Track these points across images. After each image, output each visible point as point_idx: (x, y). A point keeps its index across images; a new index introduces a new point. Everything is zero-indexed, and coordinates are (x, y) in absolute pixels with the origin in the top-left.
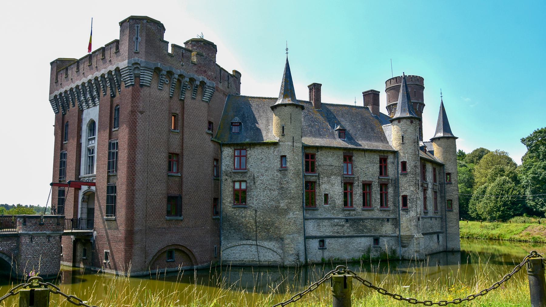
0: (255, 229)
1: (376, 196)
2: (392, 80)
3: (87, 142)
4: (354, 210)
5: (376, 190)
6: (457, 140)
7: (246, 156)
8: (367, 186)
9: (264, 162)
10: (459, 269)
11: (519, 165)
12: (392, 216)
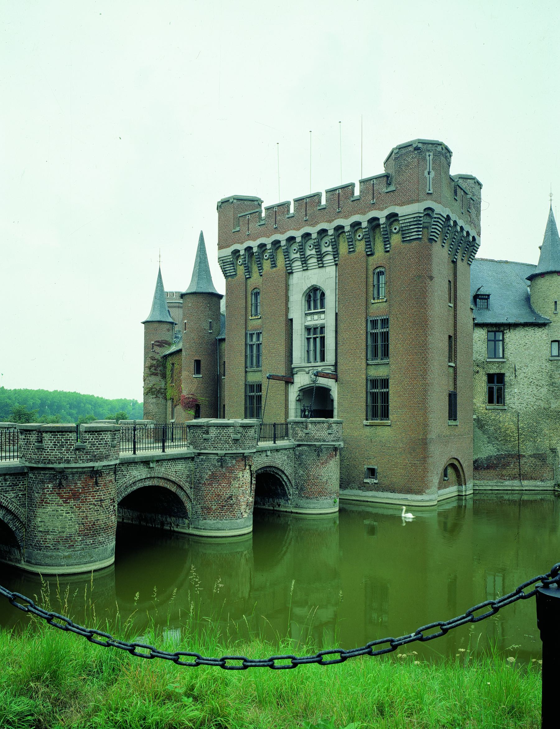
3: (304, 318)
7: (503, 340)
9: (528, 348)
10: (292, 589)
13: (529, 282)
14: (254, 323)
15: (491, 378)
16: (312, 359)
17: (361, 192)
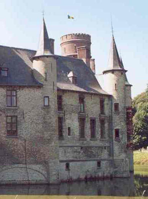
0: (25, 155)
1: (98, 129)
2: (68, 36)
4: (86, 140)
5: (98, 124)
6: (131, 87)
8: (93, 121)
11: (18, 93)
12: (107, 145)
16: (98, 135)
17: (144, 191)
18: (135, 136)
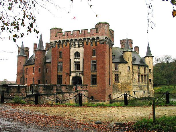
1: (144, 79)
5: (144, 77)
8: (142, 76)
11: (119, 65)
12: (147, 85)
13: (122, 53)
14: (60, 59)
15: (115, 75)
16: (144, 82)
18: (24, 98)
